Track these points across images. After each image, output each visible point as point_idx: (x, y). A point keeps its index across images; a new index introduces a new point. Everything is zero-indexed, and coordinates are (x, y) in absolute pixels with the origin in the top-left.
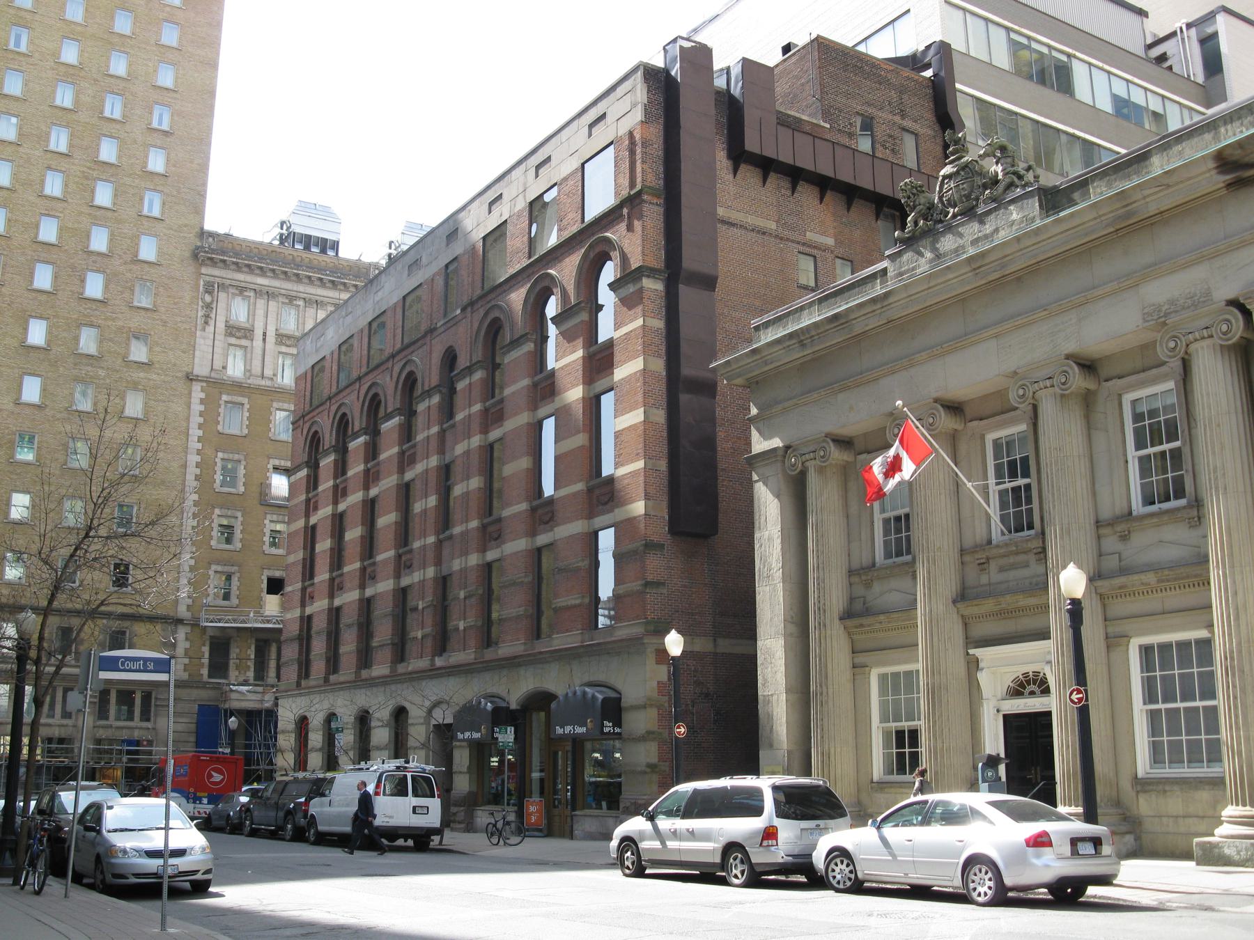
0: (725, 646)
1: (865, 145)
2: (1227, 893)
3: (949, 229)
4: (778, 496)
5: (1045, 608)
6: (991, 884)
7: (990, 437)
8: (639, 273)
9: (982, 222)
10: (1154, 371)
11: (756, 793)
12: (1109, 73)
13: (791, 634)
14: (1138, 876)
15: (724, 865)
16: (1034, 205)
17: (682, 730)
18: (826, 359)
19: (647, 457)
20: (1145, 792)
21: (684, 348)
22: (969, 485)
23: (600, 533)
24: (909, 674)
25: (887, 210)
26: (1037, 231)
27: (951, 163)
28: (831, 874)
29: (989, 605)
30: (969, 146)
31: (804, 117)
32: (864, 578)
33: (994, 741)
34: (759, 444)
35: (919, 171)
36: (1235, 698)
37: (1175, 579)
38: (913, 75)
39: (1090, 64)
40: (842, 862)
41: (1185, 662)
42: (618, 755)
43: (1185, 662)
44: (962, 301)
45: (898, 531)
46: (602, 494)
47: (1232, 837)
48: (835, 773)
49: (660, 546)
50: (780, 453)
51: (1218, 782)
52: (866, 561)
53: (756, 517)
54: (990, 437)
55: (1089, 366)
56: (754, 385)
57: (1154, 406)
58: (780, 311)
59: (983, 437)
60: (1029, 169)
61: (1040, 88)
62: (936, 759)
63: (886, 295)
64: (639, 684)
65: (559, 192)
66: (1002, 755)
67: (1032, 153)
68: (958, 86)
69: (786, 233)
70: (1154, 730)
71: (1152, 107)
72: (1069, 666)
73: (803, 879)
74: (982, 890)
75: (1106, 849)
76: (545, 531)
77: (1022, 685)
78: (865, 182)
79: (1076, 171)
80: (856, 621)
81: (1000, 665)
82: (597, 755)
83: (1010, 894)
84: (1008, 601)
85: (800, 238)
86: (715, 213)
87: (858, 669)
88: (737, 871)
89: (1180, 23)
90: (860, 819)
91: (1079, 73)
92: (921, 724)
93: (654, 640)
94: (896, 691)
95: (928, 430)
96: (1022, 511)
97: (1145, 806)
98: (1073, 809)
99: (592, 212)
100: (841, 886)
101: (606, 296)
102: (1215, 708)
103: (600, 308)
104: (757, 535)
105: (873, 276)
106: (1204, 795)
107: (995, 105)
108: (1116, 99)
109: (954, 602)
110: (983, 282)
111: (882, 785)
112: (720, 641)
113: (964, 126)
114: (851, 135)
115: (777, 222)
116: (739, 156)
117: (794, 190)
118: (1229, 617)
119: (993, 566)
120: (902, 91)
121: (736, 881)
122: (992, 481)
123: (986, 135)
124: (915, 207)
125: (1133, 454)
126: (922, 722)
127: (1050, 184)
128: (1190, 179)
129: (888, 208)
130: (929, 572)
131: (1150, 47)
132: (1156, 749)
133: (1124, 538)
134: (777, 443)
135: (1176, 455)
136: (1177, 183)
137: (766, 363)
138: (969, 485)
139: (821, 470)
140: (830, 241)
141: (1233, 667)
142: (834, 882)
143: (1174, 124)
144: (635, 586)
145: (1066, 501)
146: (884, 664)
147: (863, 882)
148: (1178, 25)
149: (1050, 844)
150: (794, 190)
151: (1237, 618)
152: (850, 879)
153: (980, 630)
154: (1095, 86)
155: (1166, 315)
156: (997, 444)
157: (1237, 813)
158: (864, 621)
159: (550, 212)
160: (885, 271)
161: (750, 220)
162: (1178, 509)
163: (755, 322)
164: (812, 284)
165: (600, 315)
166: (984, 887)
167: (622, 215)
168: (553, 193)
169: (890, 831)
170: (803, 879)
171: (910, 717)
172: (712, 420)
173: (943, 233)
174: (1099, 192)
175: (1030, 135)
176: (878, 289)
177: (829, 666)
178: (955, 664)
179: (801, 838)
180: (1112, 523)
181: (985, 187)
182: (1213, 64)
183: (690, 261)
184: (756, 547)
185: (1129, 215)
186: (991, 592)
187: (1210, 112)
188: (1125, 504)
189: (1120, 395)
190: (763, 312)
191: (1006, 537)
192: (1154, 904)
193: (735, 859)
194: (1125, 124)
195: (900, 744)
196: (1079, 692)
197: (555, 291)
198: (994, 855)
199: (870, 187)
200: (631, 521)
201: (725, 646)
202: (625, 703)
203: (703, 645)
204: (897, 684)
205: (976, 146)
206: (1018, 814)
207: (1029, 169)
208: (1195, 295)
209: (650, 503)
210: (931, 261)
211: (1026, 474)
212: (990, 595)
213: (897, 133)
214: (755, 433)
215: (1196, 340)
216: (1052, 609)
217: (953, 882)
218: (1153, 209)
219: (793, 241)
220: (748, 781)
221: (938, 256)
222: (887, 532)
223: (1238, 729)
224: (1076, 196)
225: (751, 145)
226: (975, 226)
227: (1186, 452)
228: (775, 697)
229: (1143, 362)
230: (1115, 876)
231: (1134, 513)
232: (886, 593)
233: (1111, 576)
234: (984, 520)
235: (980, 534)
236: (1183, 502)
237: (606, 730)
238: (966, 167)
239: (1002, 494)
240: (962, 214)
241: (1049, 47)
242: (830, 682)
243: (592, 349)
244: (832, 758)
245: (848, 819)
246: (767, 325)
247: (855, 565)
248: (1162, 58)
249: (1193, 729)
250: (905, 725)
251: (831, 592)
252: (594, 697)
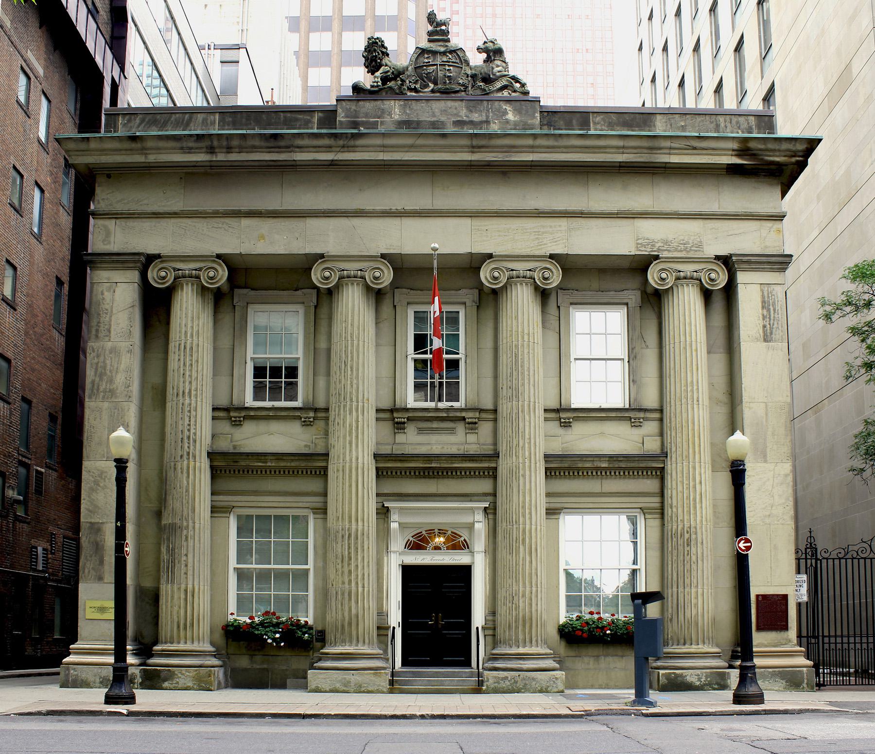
23: (396, 33)
208: (687, 243)
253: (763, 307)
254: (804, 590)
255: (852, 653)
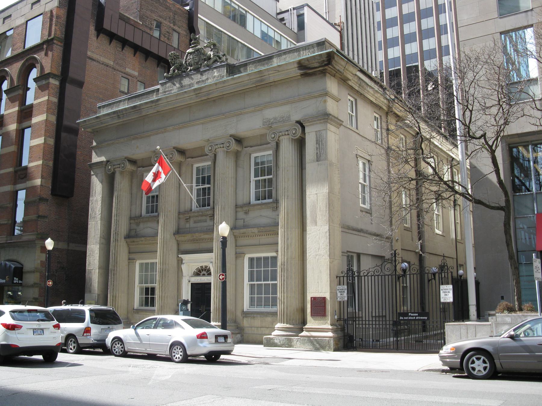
0: (73, 247)
1: (156, 34)
2: (274, 357)
3: (188, 75)
4: (102, 182)
5: (212, 239)
6: (182, 354)
7: (196, 166)
8: (49, 75)
9: (202, 75)
10: (265, 146)
11: (83, 312)
12: (261, 21)
13: (102, 243)
14: (241, 351)
15: (66, 344)
16: (224, 71)
17: (51, 283)
18: (129, 125)
19: (44, 159)
20: (246, 317)
21: (66, 112)
22: (185, 185)
23: (19, 192)
24: (152, 264)
25: (163, 63)
26: (224, 82)
27: (192, 47)
28: (113, 349)
29: (188, 237)
30: (200, 42)
31: (132, 18)
32: (136, 221)
33: (186, 294)
34: (96, 159)
35: (178, 49)
36: (284, 281)
37: (265, 232)
38: (181, 7)
39: (254, 16)
40: (119, 344)
41: (266, 266)
42: (20, 293)
43: (266, 266)
44: (189, 107)
45: (153, 202)
46: (22, 174)
47: (278, 335)
48: (118, 305)
49: (47, 200)
50: (104, 163)
51: (275, 314)
52: (138, 214)
53: (91, 191)
54: (196, 166)
55: (239, 141)
56: (96, 133)
57: (263, 160)
58: (110, 101)
59: (192, 166)
60: (224, 55)
61: (233, 22)
62: (162, 300)
63: (158, 100)
64: (32, 261)
65: (14, 32)
66: (190, 300)
67: (226, 49)
68: (199, 15)
69: (117, 67)
70: (252, 292)
71: (276, 38)
72: (220, 264)
73: (101, 350)
74: (177, 356)
75: (229, 340)
76: (21, 183)
77: (200, 271)
78: (154, 50)
79: (243, 59)
80: (131, 240)
81: (192, 262)
82: (10, 293)
83: (189, 358)
84: (197, 236)
85: (123, 70)
86: (86, 54)
87: (131, 260)
88: (72, 346)
89: (290, 7)
90: (128, 325)
91: (249, 19)
92: (156, 285)
93: (41, 242)
94: (147, 271)
95: (169, 160)
96: (206, 198)
97: (246, 323)
98: (217, 324)
99: (29, 44)
100: (118, 354)
101: (32, 84)
102: (276, 284)
103: (28, 89)
104: (91, 199)
105: (153, 92)
106: (269, 319)
107: (213, 26)
108: (263, 33)
109: (174, 234)
110: (200, 100)
111: (138, 311)
112: (71, 244)
113: (199, 33)
114: (151, 29)
115: (114, 62)
116: (100, 30)
117: (123, 49)
118: (284, 248)
119: (192, 220)
120: (175, 13)
121: (71, 351)
122: (194, 184)
123: (208, 38)
124: (174, 64)
125: (253, 179)
126: (157, 285)
127: (232, 63)
128: (288, 70)
129: (163, 63)
130: (164, 221)
131: (278, 14)
132: (252, 300)
133: (246, 213)
134: (103, 159)
135: (270, 181)
136: (282, 71)
137: (102, 123)
138: (185, 185)
139: (122, 173)
140: (136, 74)
141: (284, 269)
142: (115, 352)
143: (284, 47)
144: (34, 217)
145: (224, 195)
146: (142, 259)
147: (127, 352)
148: (290, 7)
149: (207, 338)
150: (123, 49)
151: (288, 249)
152: (122, 351)
153: (184, 247)
154: (255, 26)
155: (272, 123)
156: (198, 169)
157: (281, 326)
158: (135, 240)
159: (9, 41)
160: (158, 90)
161: (102, 59)
162: (269, 203)
163: (99, 105)
164: (126, 91)
165: (28, 92)
166: (178, 355)
167: (43, 48)
168: (11, 32)
169: (140, 331)
170: (101, 350)
171: (152, 282)
172: (75, 146)
173: (185, 77)
174: (251, 69)
175: (226, 41)
176: (154, 97)
177: (118, 259)
178: (173, 261)
179: (101, 332)
180: (242, 207)
181: (205, 60)
182: (301, 26)
183: (72, 73)
184: (90, 204)
185: (262, 81)
186: (190, 231)
187: (298, 44)
188: (248, 198)
189: (250, 154)
190: (103, 100)
191: (198, 209)
192: (246, 362)
193: (71, 341)
194: (264, 43)
195: (147, 293)
196: (223, 275)
197: (7, 78)
198: (183, 341)
199: (156, 53)
200: (34, 187)
201: (73, 247)
202: (25, 269)
203: (63, 245)
204: (147, 268)
205: (204, 42)
206: (194, 325)
207: (224, 55)
208: (284, 117)
209: (44, 180)
210: (178, 88)
211: (209, 183)
212: (189, 232)
213: (171, 31)
214: (94, 154)
215: (283, 135)
216: (214, 241)
217: (165, 352)
218: (271, 80)
219: (120, 71)
220: (79, 307)
221: (182, 87)
222: (148, 202)
223: (284, 293)
224: (242, 69)
225: (106, 25)
226: (199, 76)
227: (274, 180)
228: (93, 271)
229: (261, 142)
230: (232, 351)
231: (251, 203)
232: (145, 228)
233: (240, 228)
234: (189, 200)
235: (188, 206)
236: (271, 200)
237: (15, 282)
238: (198, 50)
239: (198, 190)
240: (194, 70)
241: (239, 6)
242: (118, 265)
243: (23, 107)
244: (117, 298)
245: (122, 325)
246: (104, 107)
247: (133, 216)
248: (282, 20)
249: (267, 293)
250: (150, 285)
251: (121, 226)
252: (10, 266)
253: (317, 143)
254: (345, 294)
255: (371, 330)
